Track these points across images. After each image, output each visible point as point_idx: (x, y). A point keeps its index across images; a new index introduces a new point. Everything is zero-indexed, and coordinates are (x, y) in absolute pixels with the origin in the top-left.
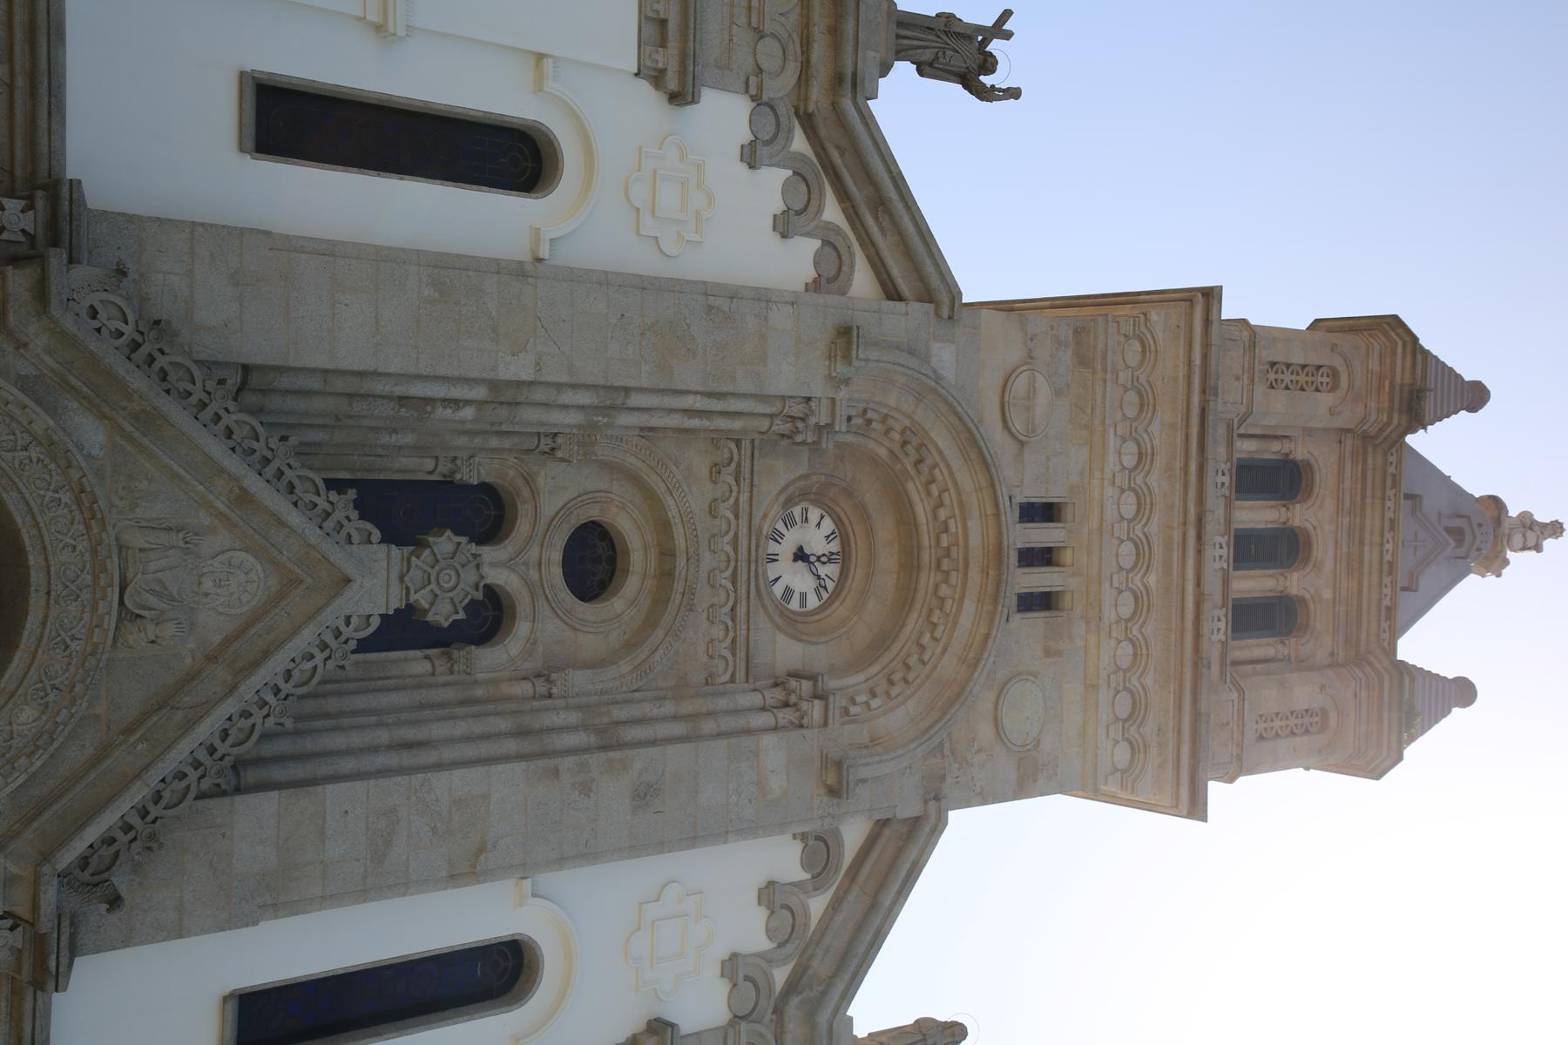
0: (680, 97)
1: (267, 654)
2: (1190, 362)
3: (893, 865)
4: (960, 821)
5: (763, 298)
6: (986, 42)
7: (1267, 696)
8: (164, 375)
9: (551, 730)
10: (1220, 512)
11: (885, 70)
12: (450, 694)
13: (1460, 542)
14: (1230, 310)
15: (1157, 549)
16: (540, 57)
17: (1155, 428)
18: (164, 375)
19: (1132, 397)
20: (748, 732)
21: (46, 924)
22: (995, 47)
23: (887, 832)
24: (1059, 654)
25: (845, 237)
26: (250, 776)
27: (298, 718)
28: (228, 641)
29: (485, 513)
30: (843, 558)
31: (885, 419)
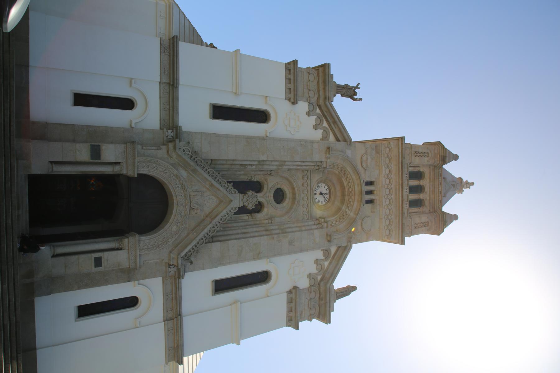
1: (217, 215)
2: (399, 152)
3: (341, 256)
4: (356, 248)
5: (312, 142)
6: (355, 89)
7: (417, 219)
8: (197, 162)
9: (272, 230)
10: (406, 182)
11: (335, 96)
12: (252, 223)
13: (454, 187)
14: (406, 141)
15: (394, 190)
16: (266, 97)
17: (392, 166)
18: (197, 162)
19: (387, 159)
20: (311, 229)
21: (180, 267)
22: (357, 90)
23: (340, 249)
24: (374, 212)
26: (215, 239)
27: (223, 228)
28: (210, 213)
29: (257, 187)
30: (330, 193)
31: (337, 165)
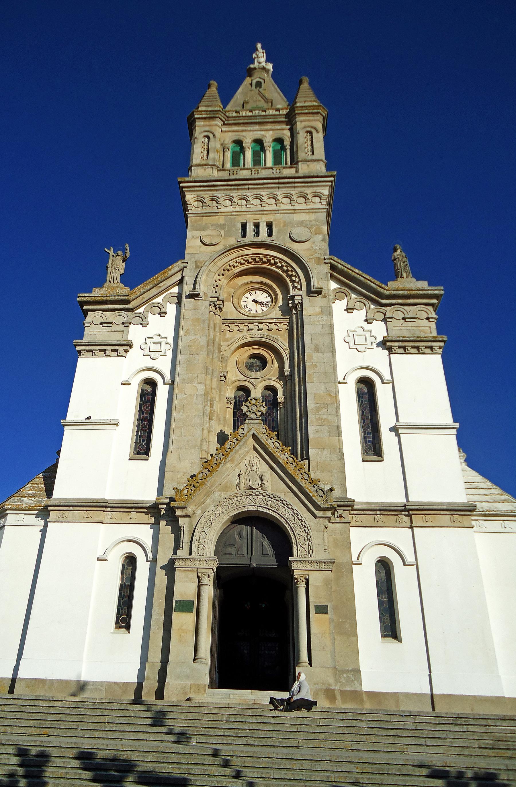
0: (130, 345)
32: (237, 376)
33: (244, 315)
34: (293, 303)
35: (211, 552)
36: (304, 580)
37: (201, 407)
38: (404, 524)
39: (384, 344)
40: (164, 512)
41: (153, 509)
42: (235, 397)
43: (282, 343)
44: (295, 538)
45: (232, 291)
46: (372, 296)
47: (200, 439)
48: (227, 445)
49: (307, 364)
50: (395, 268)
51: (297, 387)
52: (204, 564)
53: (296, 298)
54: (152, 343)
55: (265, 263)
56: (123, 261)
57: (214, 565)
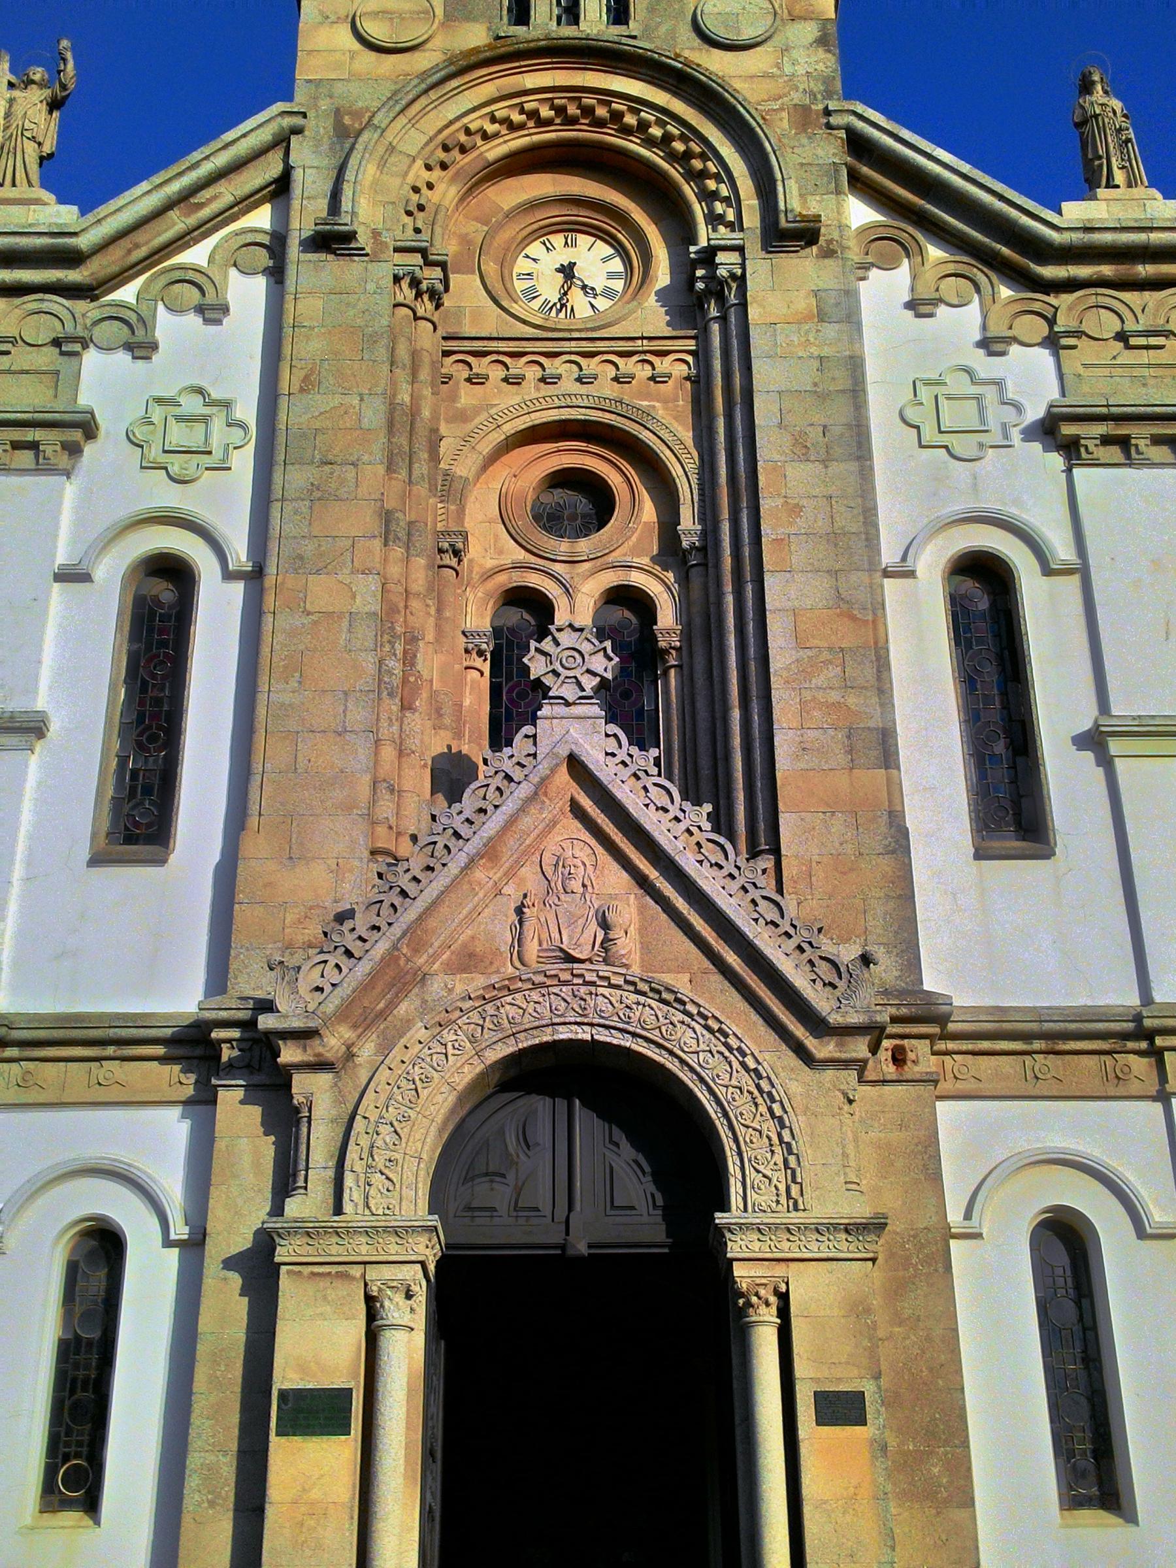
2: (727, 91)
25: (226, 239)
32: (501, 552)
33: (524, 322)
34: (711, 277)
35: (412, 1202)
36: (773, 1299)
37: (368, 662)
38: (1135, 1087)
39: (1050, 431)
40: (235, 1058)
41: (192, 1046)
42: (497, 632)
43: (671, 430)
44: (736, 1140)
45: (477, 231)
46: (1005, 251)
47: (367, 779)
48: (469, 801)
49: (765, 504)
50: (1085, 154)
51: (728, 588)
52: (393, 1248)
53: (721, 257)
54: (172, 421)
55: (599, 123)
56: (54, 105)
57: (428, 1250)
